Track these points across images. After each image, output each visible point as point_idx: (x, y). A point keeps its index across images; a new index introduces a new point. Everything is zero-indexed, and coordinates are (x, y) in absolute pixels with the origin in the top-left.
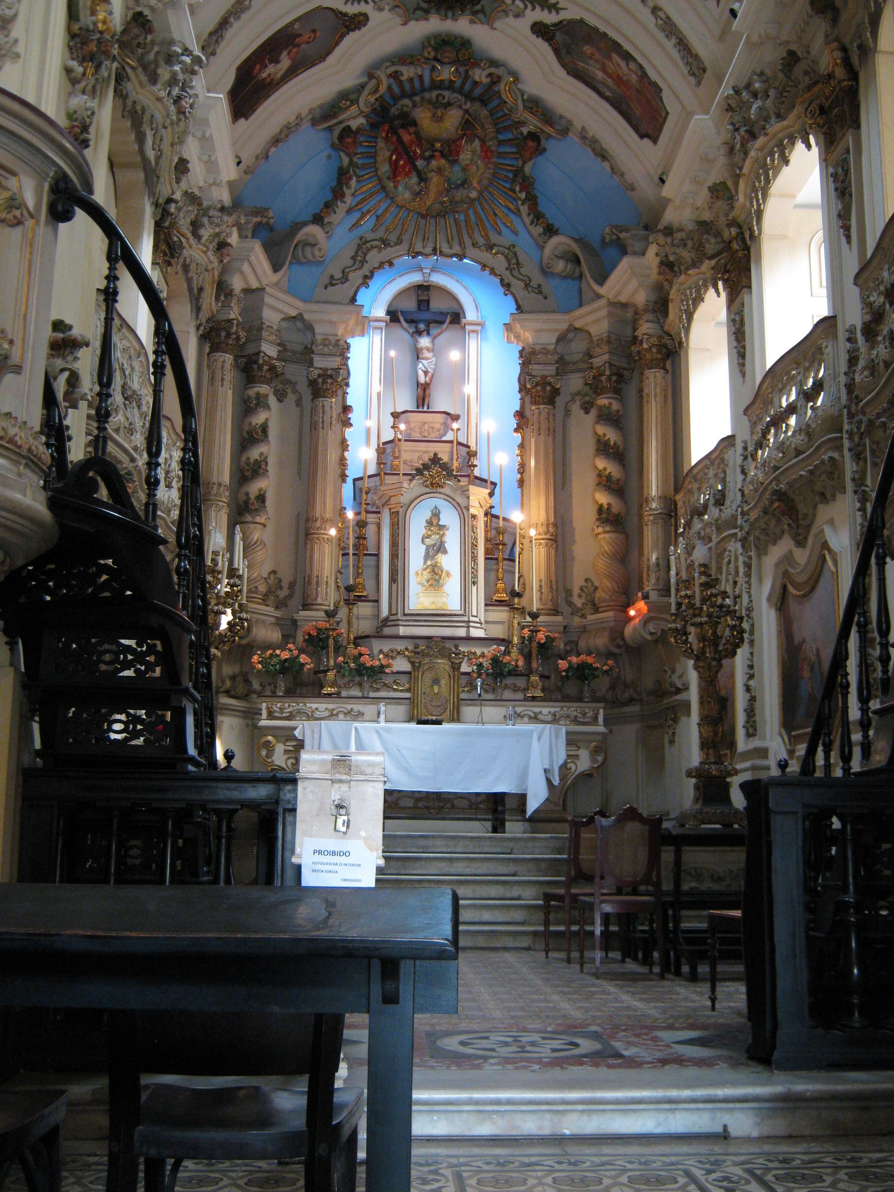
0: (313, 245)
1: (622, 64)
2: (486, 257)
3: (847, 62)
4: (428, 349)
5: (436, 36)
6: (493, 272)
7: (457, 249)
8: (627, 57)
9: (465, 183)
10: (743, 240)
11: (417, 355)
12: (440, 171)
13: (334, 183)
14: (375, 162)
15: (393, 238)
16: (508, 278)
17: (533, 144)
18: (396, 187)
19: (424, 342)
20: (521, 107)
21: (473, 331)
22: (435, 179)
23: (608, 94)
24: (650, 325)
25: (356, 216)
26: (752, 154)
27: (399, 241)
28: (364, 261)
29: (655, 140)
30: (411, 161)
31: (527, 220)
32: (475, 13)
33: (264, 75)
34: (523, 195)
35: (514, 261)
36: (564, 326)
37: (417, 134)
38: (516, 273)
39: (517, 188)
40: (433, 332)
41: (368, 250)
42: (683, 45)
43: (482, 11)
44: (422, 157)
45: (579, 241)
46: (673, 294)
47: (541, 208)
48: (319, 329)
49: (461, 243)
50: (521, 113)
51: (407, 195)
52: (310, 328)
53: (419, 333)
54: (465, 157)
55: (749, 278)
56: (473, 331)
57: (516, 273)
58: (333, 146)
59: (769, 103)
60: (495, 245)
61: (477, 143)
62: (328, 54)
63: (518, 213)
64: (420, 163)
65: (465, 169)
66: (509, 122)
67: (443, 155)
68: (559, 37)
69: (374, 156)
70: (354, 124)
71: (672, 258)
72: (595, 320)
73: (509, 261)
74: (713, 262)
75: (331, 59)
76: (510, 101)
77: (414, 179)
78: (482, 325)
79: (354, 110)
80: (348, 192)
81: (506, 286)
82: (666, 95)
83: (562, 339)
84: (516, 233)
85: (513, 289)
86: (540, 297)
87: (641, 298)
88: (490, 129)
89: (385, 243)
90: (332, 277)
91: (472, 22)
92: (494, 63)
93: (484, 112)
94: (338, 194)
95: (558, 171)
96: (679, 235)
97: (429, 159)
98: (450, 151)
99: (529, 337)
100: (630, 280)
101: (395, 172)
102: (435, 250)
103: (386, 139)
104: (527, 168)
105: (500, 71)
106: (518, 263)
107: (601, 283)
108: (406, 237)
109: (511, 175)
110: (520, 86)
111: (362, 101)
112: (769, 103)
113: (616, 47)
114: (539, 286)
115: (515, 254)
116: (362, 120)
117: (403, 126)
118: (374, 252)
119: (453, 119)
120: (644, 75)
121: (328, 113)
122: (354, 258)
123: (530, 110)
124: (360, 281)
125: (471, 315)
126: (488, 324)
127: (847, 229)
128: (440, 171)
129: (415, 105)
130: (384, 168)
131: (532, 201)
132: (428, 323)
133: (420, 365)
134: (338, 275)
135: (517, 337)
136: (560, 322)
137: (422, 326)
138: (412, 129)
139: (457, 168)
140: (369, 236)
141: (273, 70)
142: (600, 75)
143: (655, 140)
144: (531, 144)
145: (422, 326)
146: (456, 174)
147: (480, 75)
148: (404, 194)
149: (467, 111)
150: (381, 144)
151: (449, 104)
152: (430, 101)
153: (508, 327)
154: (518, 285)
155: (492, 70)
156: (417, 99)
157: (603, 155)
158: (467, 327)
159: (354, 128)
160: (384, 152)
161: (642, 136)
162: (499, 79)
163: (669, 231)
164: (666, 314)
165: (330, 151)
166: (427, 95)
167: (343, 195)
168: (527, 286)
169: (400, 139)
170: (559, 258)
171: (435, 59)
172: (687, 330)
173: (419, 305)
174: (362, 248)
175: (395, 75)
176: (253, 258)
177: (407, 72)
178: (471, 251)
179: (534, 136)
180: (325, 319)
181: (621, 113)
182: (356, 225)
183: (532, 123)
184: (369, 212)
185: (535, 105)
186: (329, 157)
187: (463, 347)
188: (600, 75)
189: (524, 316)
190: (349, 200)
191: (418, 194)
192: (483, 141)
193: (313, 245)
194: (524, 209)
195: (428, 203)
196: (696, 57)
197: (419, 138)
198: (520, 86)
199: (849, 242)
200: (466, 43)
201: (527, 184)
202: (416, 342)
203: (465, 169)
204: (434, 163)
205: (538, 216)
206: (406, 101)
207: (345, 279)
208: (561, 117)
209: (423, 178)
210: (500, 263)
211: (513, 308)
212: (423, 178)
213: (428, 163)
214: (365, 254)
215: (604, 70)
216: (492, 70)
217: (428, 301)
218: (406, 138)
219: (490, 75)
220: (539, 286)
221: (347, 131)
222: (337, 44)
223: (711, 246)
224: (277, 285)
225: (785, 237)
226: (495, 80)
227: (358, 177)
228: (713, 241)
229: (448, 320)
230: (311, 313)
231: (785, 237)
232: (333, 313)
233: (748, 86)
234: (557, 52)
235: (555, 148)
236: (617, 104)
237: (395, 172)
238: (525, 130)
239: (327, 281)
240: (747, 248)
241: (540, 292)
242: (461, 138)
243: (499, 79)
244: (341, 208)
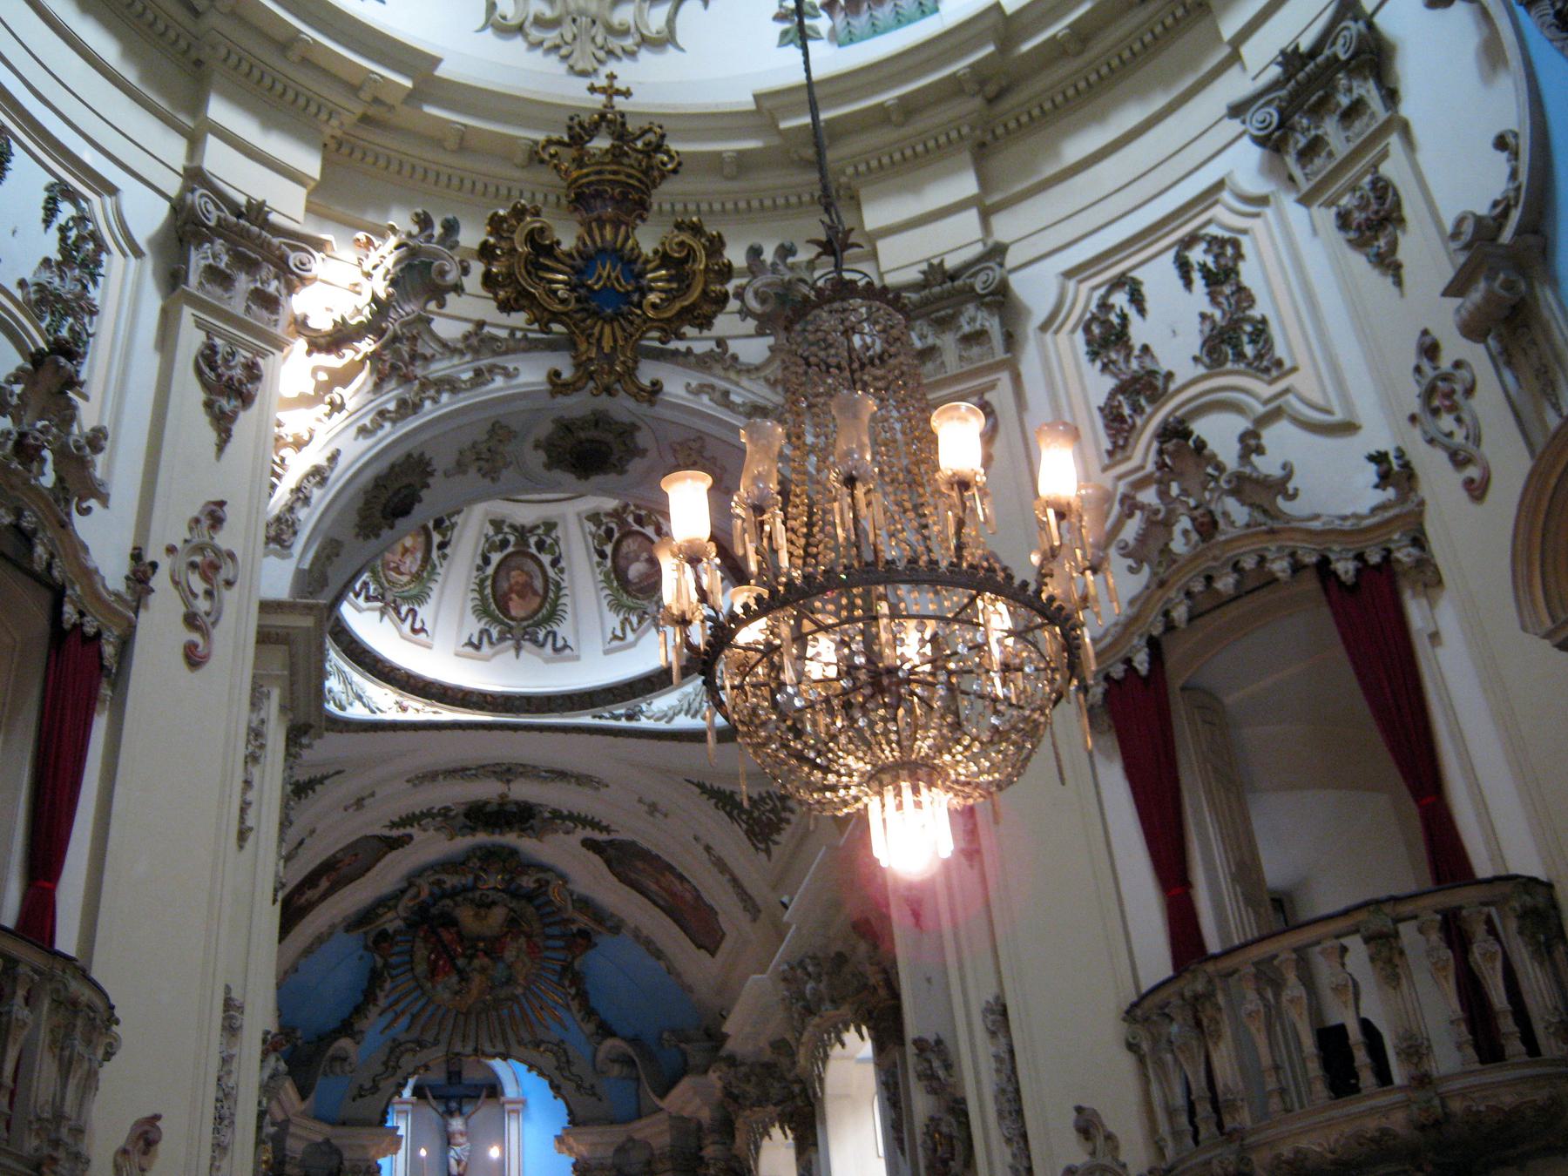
0: (344, 1059)
1: (677, 882)
2: (532, 1054)
3: (885, 971)
4: (461, 1134)
5: (480, 847)
6: (541, 1074)
7: (501, 1048)
8: (681, 878)
9: (510, 981)
10: (808, 1097)
11: (448, 1140)
12: (483, 970)
13: (365, 985)
14: (412, 961)
15: (429, 1037)
16: (558, 1079)
17: (585, 939)
18: (434, 987)
19: (457, 1124)
20: (570, 907)
21: (514, 1111)
22: (477, 980)
23: (661, 902)
24: (717, 1147)
25: (390, 1015)
26: (810, 1029)
27: (436, 1043)
28: (397, 1067)
29: (713, 954)
30: (452, 959)
31: (578, 1017)
32: (523, 830)
33: (303, 900)
34: (573, 991)
35: (563, 1059)
36: (621, 1139)
37: (459, 933)
38: (567, 1074)
39: (567, 983)
40: (467, 1109)
41: (402, 1054)
42: (735, 881)
43: (532, 828)
44: (463, 955)
45: (634, 1041)
46: (739, 1124)
47: (593, 1002)
48: (347, 1155)
49: (505, 1040)
50: (570, 912)
51: (447, 996)
52: (337, 1152)
53: (450, 1113)
54: (510, 954)
55: (815, 1135)
56: (514, 1111)
57: (567, 1074)
58: (366, 947)
59: (822, 986)
60: (542, 1042)
61: (522, 940)
62: (368, 869)
63: (568, 1008)
64: (461, 962)
65: (509, 967)
66: (557, 918)
67: (486, 954)
68: (611, 852)
69: (411, 953)
70: (390, 928)
71: (736, 1091)
72: (655, 1133)
73: (558, 1060)
74: (779, 1108)
75: (370, 874)
76: (557, 900)
77: (455, 979)
78: (524, 1102)
79: (390, 915)
80: (381, 995)
81: (556, 1088)
82: (721, 918)
83: (621, 1150)
84: (565, 1027)
85: (564, 1092)
86: (594, 1099)
87: (705, 1115)
88: (536, 926)
89: (421, 1044)
90: (361, 1087)
91: (520, 836)
92: (542, 868)
93: (530, 910)
94: (369, 996)
95: (605, 964)
96: (743, 1069)
97: (471, 958)
98: (494, 949)
99: (583, 1150)
100: (692, 1099)
101: (433, 971)
102: (476, 1050)
103: (426, 940)
104: (576, 964)
105: (549, 876)
106: (568, 1062)
107: (663, 1094)
108: (444, 1037)
109: (558, 968)
110: (570, 886)
111: (400, 908)
112: (822, 986)
113: (670, 868)
114: (592, 1087)
115: (565, 1051)
116: (399, 923)
117: (443, 925)
118: (408, 1057)
119: (498, 915)
120: (698, 897)
121: (363, 919)
122: (385, 1064)
123: (580, 911)
124: (393, 1089)
125: (510, 1091)
126: (531, 1101)
127: (900, 1141)
128: (483, 970)
129: (456, 905)
130: (421, 968)
131: (582, 996)
132: (460, 1099)
133: (452, 1153)
134: (368, 1085)
135: (570, 1150)
136: (617, 1134)
137: (453, 1105)
138: (453, 930)
139: (501, 966)
140: (402, 1037)
141: (311, 894)
142: (654, 887)
143: (713, 954)
144: (579, 940)
145: (453, 1105)
146: (500, 972)
147: (528, 882)
148: (443, 995)
149: (512, 910)
150: (419, 944)
151: (494, 903)
152: (472, 901)
153: (560, 1140)
154: (568, 1087)
155: (541, 875)
156: (459, 899)
157: (658, 954)
158: (508, 1107)
159: (390, 931)
160: (421, 951)
161: (699, 947)
162: (548, 882)
163: (732, 1061)
164: (733, 1137)
165: (361, 952)
166: (470, 895)
167: (375, 999)
168: (579, 1087)
169: (440, 940)
170: (613, 1061)
171: (481, 868)
172: (756, 1160)
173: (449, 1078)
174: (396, 1049)
175: (439, 883)
176: (282, 1095)
177: (451, 881)
178: (515, 1049)
179: (584, 934)
180: (350, 1141)
181: (676, 921)
182: (388, 1027)
183: (583, 921)
184: (403, 1012)
185: (584, 904)
186: (361, 958)
187: (502, 1140)
188: (654, 887)
189: (577, 1130)
190: (383, 1002)
191: (456, 993)
192: (529, 937)
193: (344, 1059)
194: (575, 1005)
195: (470, 1002)
196: (750, 897)
197: (461, 937)
198: (570, 886)
199: (902, 1150)
200: (513, 852)
201: (577, 979)
202: (446, 1125)
203: (509, 967)
204: (476, 963)
205: (589, 1012)
206: (448, 902)
207: (375, 1089)
208: (612, 915)
209: (464, 977)
210: (549, 1061)
211: (563, 1118)
212: (464, 977)
213: (469, 964)
214: (398, 1058)
215: (657, 882)
216: (541, 875)
217: (459, 1074)
218: (446, 936)
219: (538, 881)
220: (592, 1087)
221: (383, 936)
222: (378, 860)
223: (776, 1090)
224: (304, 1114)
225: (848, 1096)
226: (543, 884)
227: (392, 978)
228: (776, 1084)
229: (484, 1094)
230: (341, 1137)
231: (848, 1096)
232: (364, 1135)
233: (801, 964)
234: (608, 863)
235: (604, 940)
236: (670, 912)
237: (433, 971)
238: (574, 928)
239: (355, 1092)
240: (812, 1105)
241: (594, 1094)
242: (506, 934)
243: (548, 882)
244: (374, 1011)
